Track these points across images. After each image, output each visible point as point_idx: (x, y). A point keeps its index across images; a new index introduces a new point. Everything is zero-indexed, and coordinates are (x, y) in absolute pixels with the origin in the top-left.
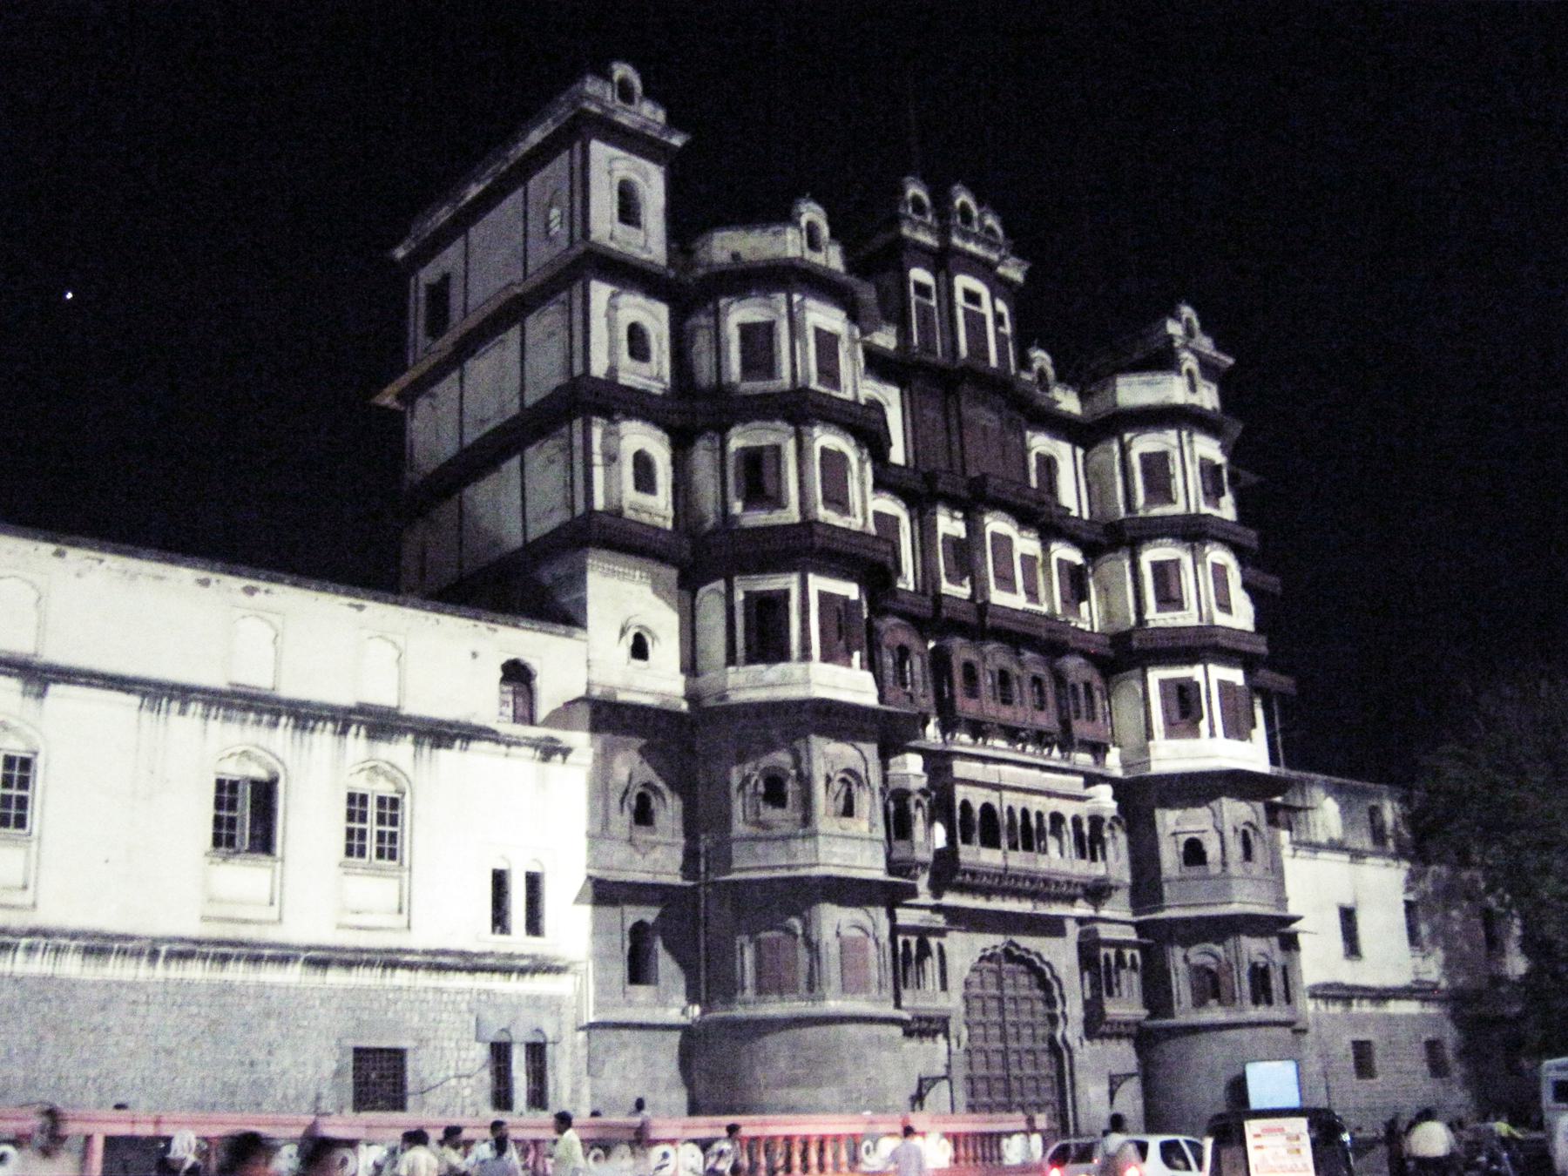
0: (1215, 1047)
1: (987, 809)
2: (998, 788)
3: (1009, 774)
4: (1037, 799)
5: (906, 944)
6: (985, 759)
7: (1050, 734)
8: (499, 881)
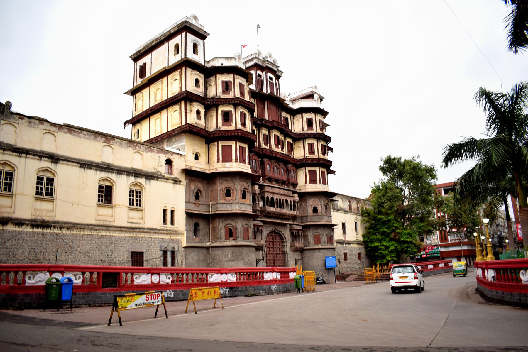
0: (319, 254)
1: (272, 198)
2: (275, 193)
3: (276, 191)
4: (283, 196)
8: (165, 211)
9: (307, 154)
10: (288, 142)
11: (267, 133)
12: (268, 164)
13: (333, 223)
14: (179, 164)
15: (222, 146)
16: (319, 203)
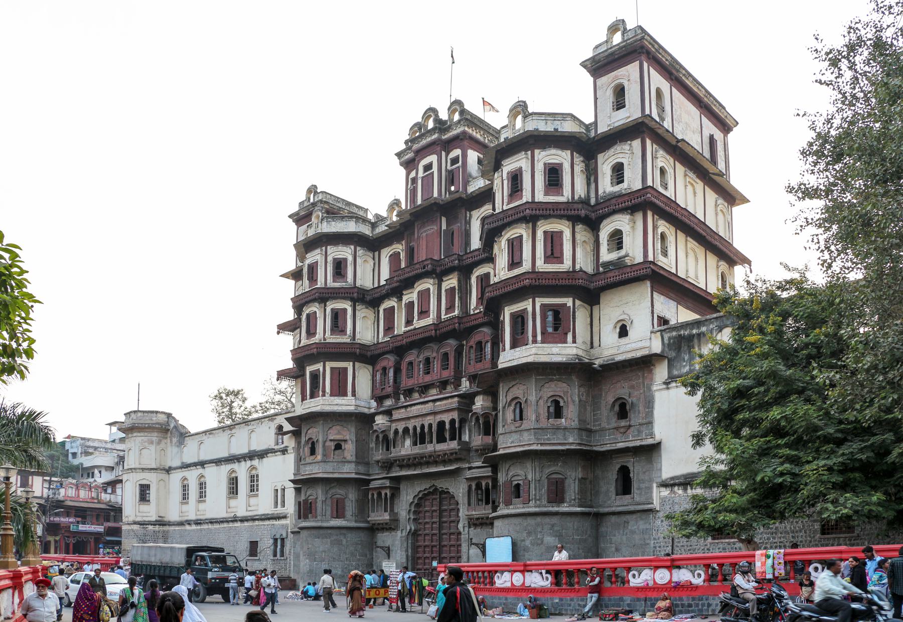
15: (332, 369)
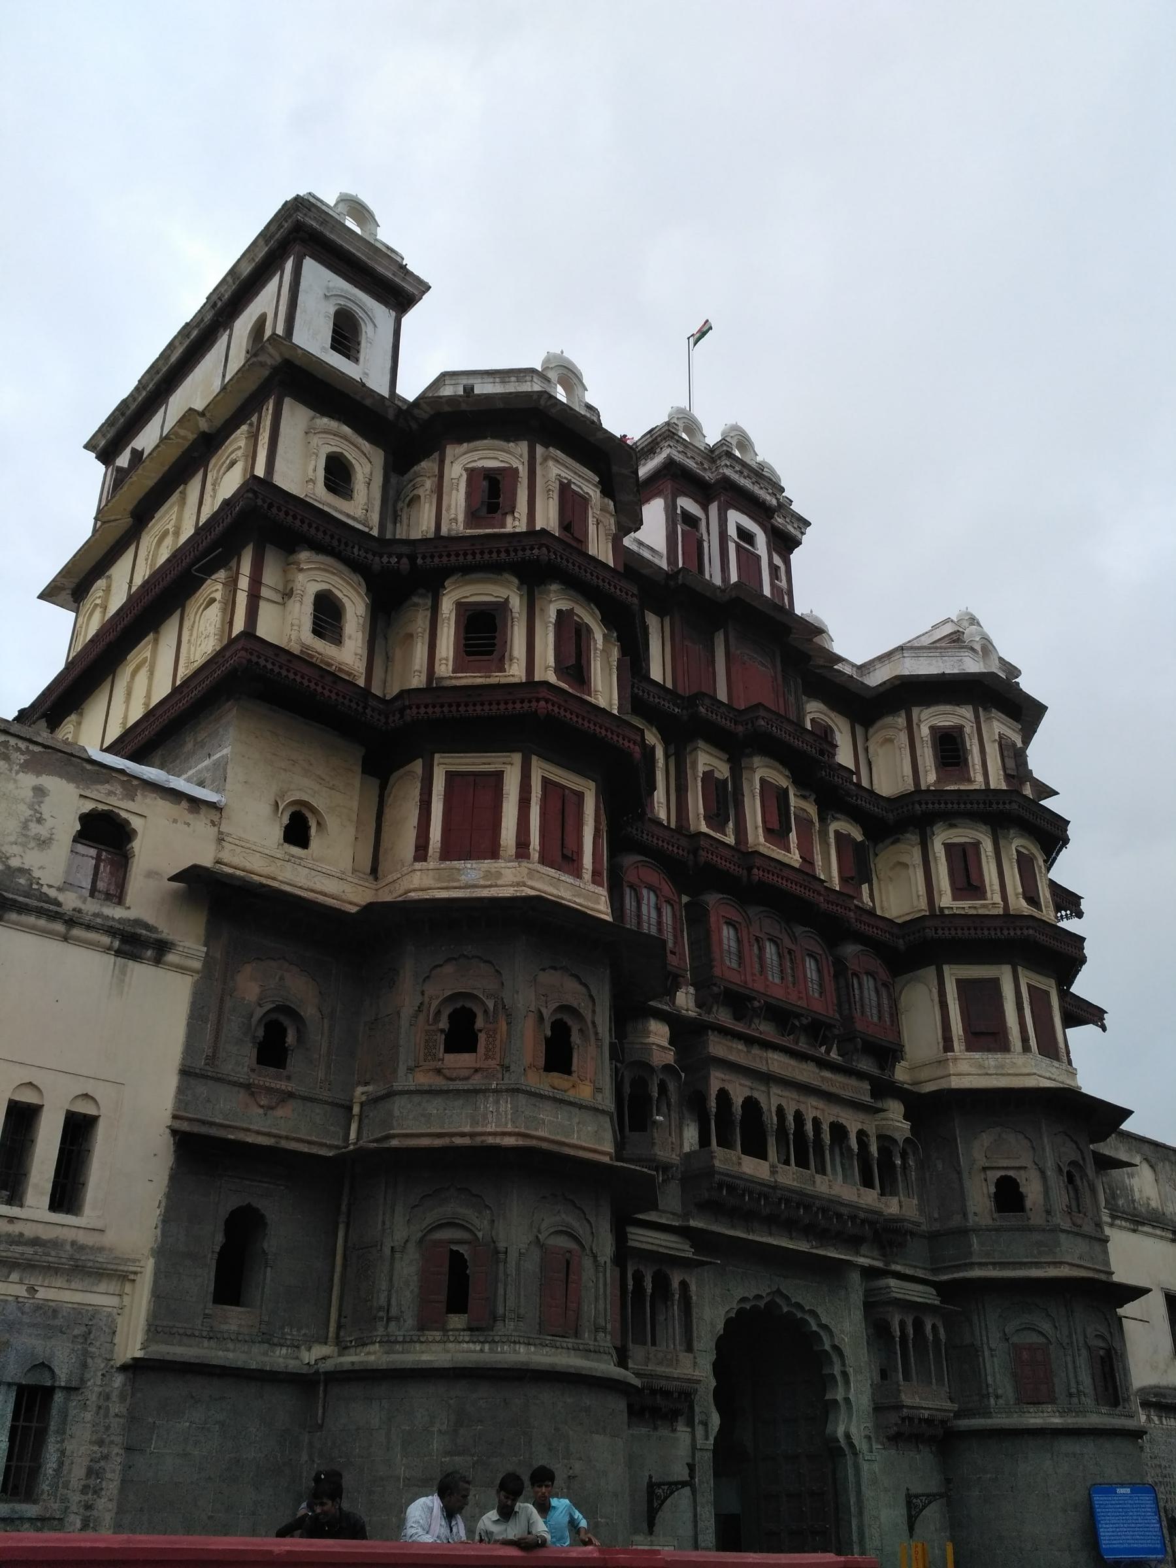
1: (751, 1104)
2: (768, 1079)
4: (813, 1101)
5: (638, 1278)
6: (750, 1041)
7: (830, 1027)
9: (946, 900)
10: (837, 832)
11: (723, 771)
12: (730, 923)
13: (1122, 1275)
14: (165, 844)
15: (450, 776)
16: (1026, 1160)
